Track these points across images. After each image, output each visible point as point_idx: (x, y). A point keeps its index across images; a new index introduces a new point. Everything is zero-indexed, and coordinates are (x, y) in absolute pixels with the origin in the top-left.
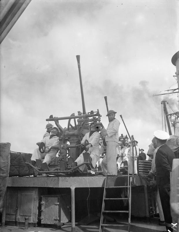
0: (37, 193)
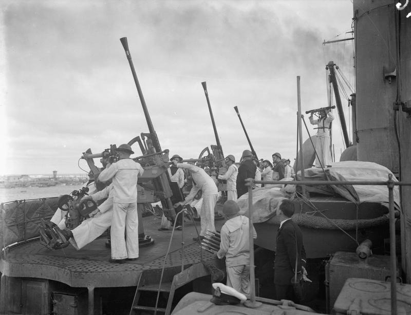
0: (47, 286)
